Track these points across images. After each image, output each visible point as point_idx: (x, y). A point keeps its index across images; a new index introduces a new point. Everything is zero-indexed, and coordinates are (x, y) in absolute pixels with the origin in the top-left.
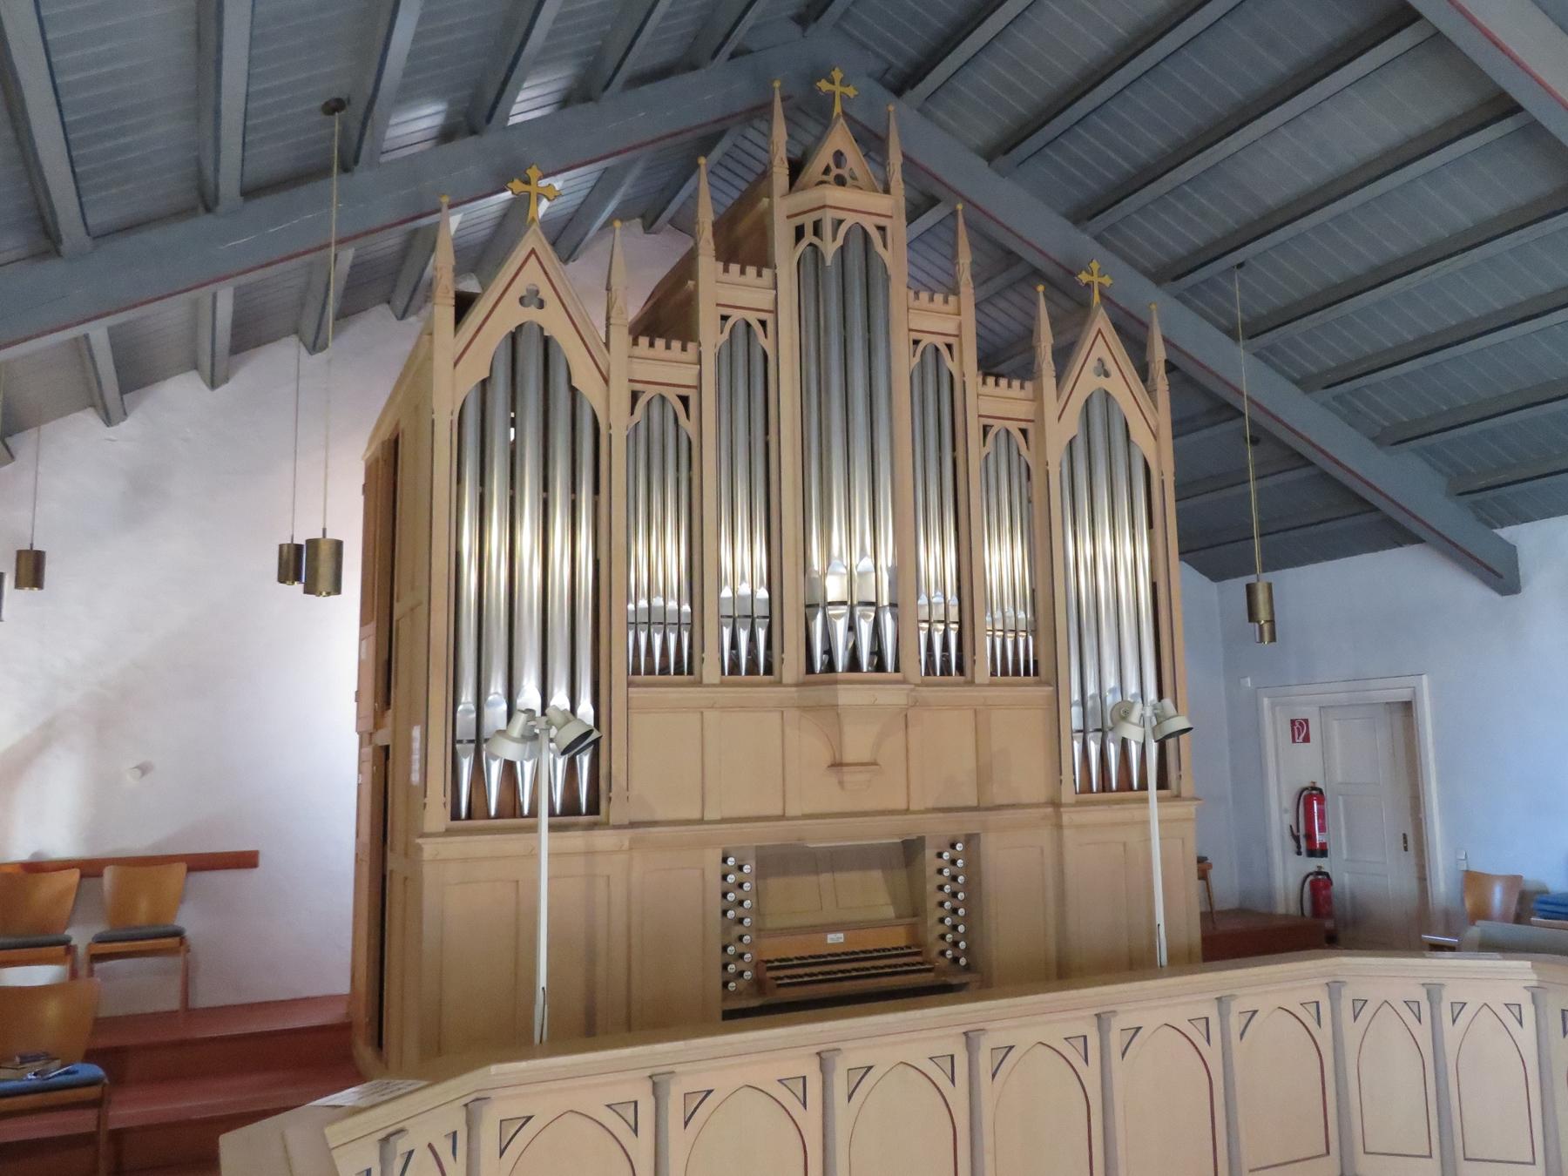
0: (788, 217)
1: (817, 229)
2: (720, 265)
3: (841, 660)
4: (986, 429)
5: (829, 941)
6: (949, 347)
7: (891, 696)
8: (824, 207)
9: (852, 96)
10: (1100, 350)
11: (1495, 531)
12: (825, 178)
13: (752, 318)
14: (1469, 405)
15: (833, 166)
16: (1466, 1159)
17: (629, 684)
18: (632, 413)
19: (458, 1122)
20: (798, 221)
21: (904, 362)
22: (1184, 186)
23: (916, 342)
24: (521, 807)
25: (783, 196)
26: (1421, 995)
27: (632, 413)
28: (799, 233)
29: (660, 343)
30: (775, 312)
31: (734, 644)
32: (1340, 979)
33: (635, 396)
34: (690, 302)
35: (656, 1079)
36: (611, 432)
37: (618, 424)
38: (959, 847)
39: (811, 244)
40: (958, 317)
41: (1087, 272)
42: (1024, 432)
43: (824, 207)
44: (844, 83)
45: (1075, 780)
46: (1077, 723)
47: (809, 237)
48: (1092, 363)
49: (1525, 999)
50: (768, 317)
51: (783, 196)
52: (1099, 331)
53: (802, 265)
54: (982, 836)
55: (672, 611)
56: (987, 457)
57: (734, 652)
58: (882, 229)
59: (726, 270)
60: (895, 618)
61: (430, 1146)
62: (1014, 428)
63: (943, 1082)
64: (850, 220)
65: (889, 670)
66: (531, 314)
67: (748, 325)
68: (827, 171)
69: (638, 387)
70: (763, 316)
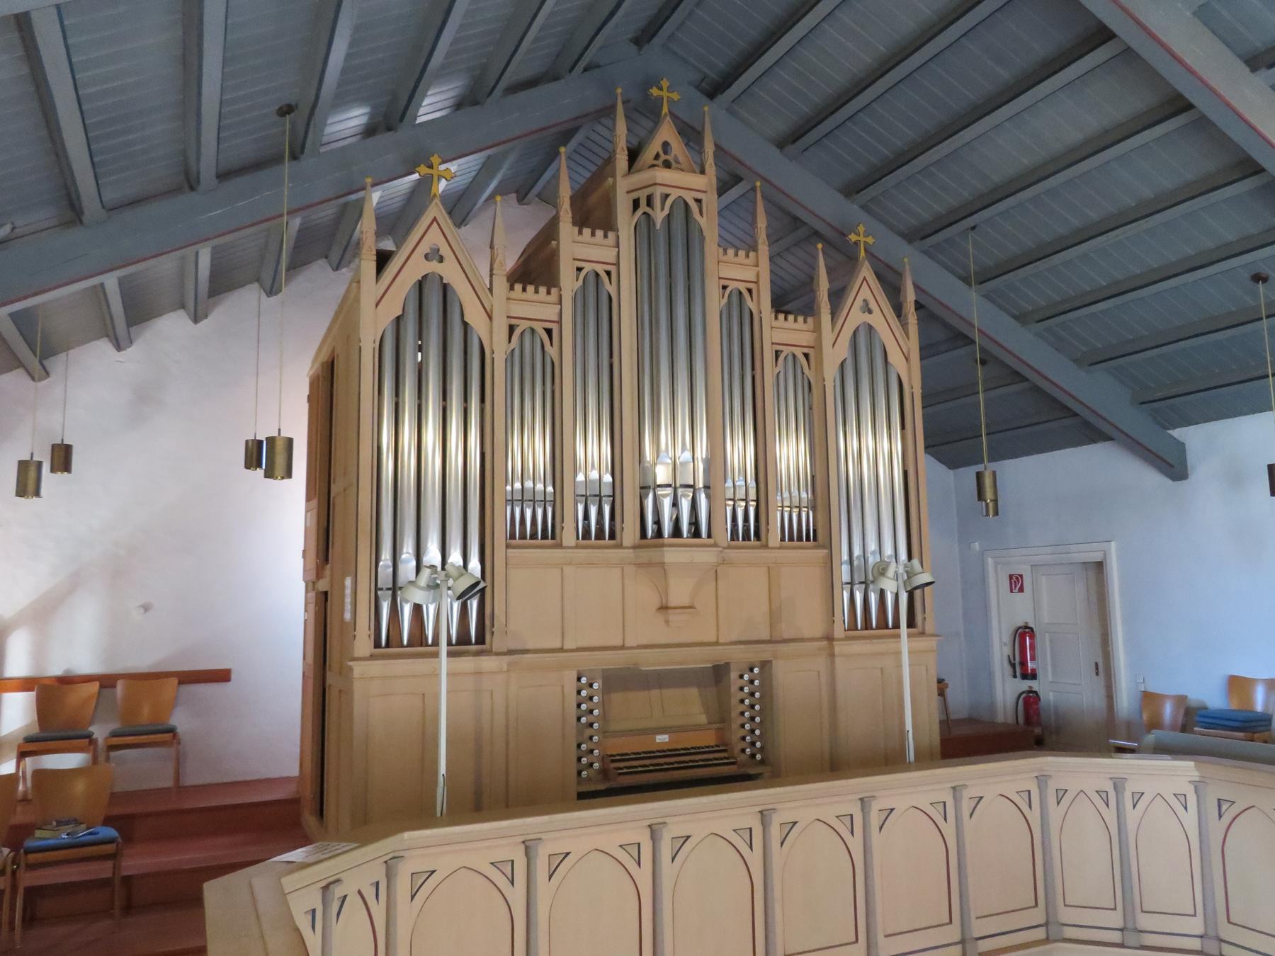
3: (667, 527)
4: (777, 353)
5: (657, 741)
6: (750, 291)
7: (704, 556)
10: (865, 293)
12: (656, 162)
13: (600, 269)
15: (661, 153)
17: (508, 546)
20: (635, 195)
21: (715, 302)
25: (624, 176)
26: (1109, 787)
28: (636, 204)
33: (512, 329)
36: (494, 355)
37: (499, 348)
38: (756, 670)
39: (645, 213)
42: (806, 356)
47: (643, 207)
48: (859, 302)
50: (612, 269)
52: (865, 279)
54: (774, 662)
57: (586, 522)
58: (698, 201)
59: (580, 233)
60: (708, 497)
61: (359, 892)
64: (675, 193)
66: (434, 267)
68: (657, 157)
69: (514, 322)
70: (608, 268)
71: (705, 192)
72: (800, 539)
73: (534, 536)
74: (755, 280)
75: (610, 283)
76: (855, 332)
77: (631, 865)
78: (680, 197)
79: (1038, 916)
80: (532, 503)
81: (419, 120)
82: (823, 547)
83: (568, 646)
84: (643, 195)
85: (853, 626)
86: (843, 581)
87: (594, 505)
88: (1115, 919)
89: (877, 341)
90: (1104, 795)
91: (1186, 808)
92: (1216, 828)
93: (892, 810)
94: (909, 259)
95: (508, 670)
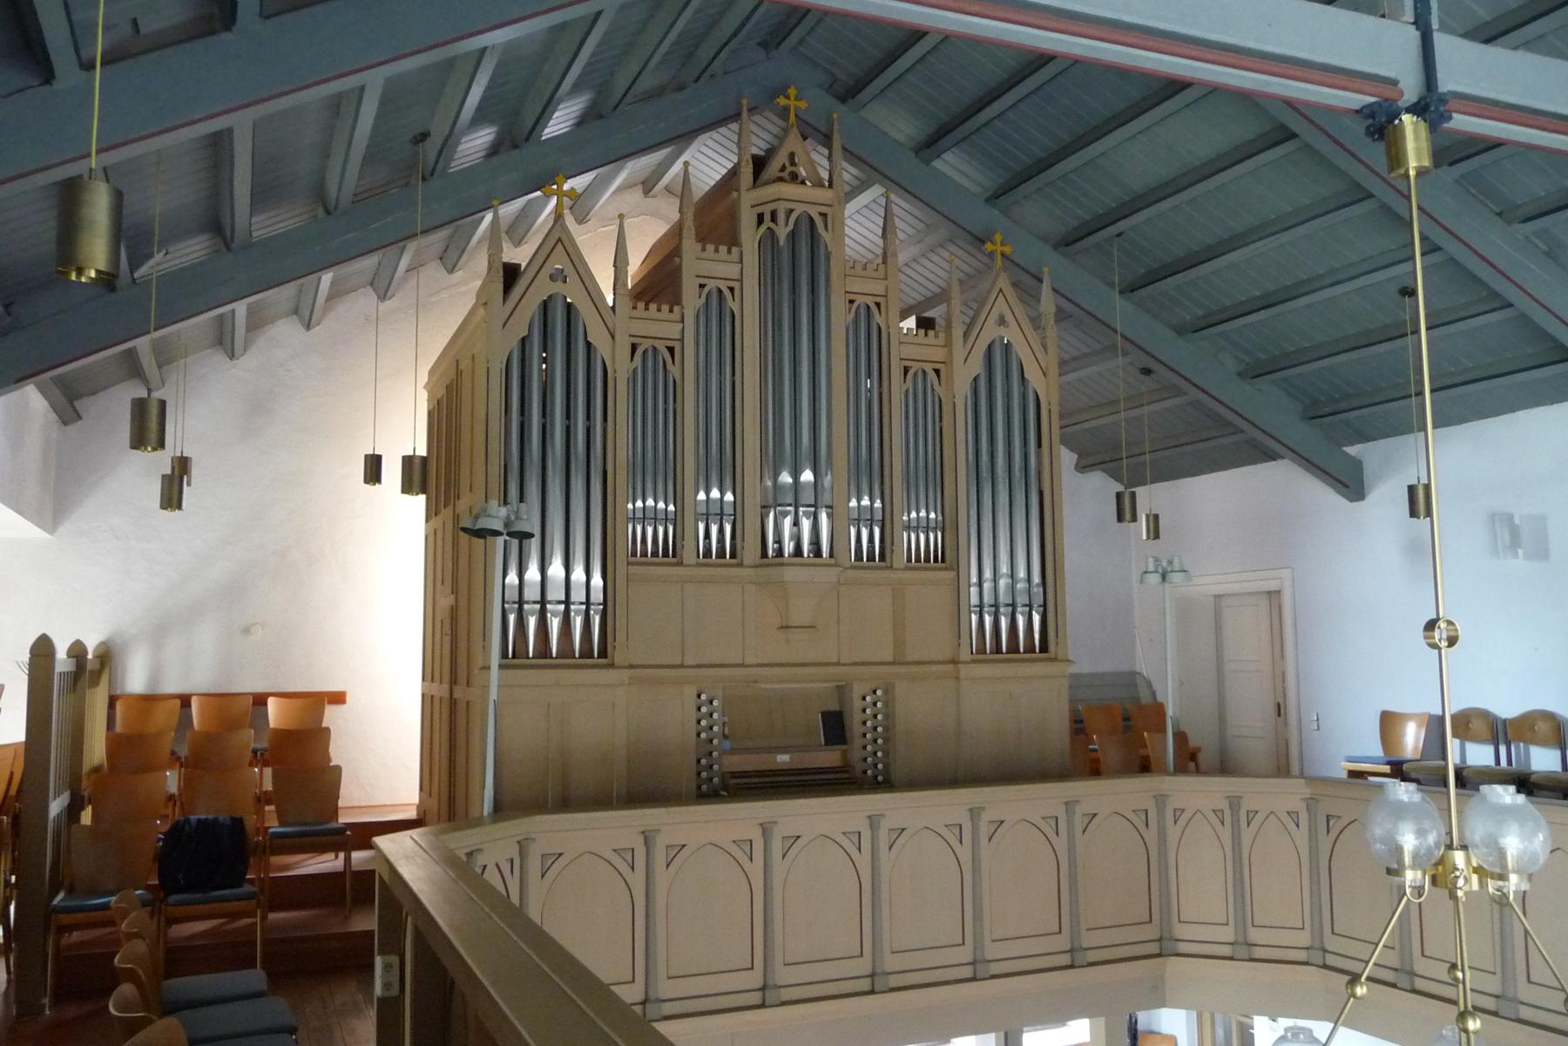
0: (753, 207)
1: (774, 217)
2: (699, 246)
3: (789, 547)
4: (906, 370)
5: (778, 760)
6: (878, 305)
7: (827, 576)
8: (779, 199)
9: (803, 108)
10: (1001, 306)
11: (1345, 449)
12: (782, 174)
13: (723, 285)
14: (1310, 347)
15: (787, 165)
16: (1253, 926)
17: (628, 564)
18: (632, 360)
19: (514, 852)
20: (760, 210)
21: (840, 317)
22: (1070, 175)
23: (851, 302)
24: (551, 653)
25: (747, 190)
26: (1224, 805)
27: (632, 360)
28: (760, 219)
29: (653, 307)
30: (741, 281)
31: (707, 535)
32: (1164, 793)
33: (634, 348)
34: (678, 271)
35: (647, 834)
36: (616, 375)
37: (622, 368)
38: (879, 692)
39: (769, 228)
40: (884, 282)
41: (992, 242)
42: (937, 371)
43: (779, 199)
44: (797, 99)
45: (971, 644)
46: (974, 600)
47: (767, 223)
48: (994, 316)
49: (1301, 808)
50: (736, 285)
51: (747, 190)
52: (1001, 290)
53: (762, 244)
55: (661, 510)
56: (907, 391)
57: (707, 541)
58: (824, 215)
59: (704, 249)
60: (830, 516)
61: (497, 865)
62: (929, 368)
63: (853, 851)
64: (799, 209)
65: (824, 556)
66: (557, 287)
67: (720, 291)
68: (783, 169)
69: (636, 340)
70: (731, 284)
71: (830, 206)
72: (927, 560)
73: (655, 554)
74: (884, 294)
75: (734, 300)
76: (990, 346)
77: (744, 860)
78: (805, 211)
79: (1152, 932)
80: (653, 521)
81: (543, 138)
82: (951, 569)
83: (688, 662)
84: (767, 210)
85: (982, 650)
86: (972, 603)
87: (715, 524)
88: (1228, 934)
89: (1014, 356)
90: (1219, 814)
91: (1298, 826)
92: (1325, 843)
93: (1002, 822)
94: (1053, 265)
95: (629, 684)
